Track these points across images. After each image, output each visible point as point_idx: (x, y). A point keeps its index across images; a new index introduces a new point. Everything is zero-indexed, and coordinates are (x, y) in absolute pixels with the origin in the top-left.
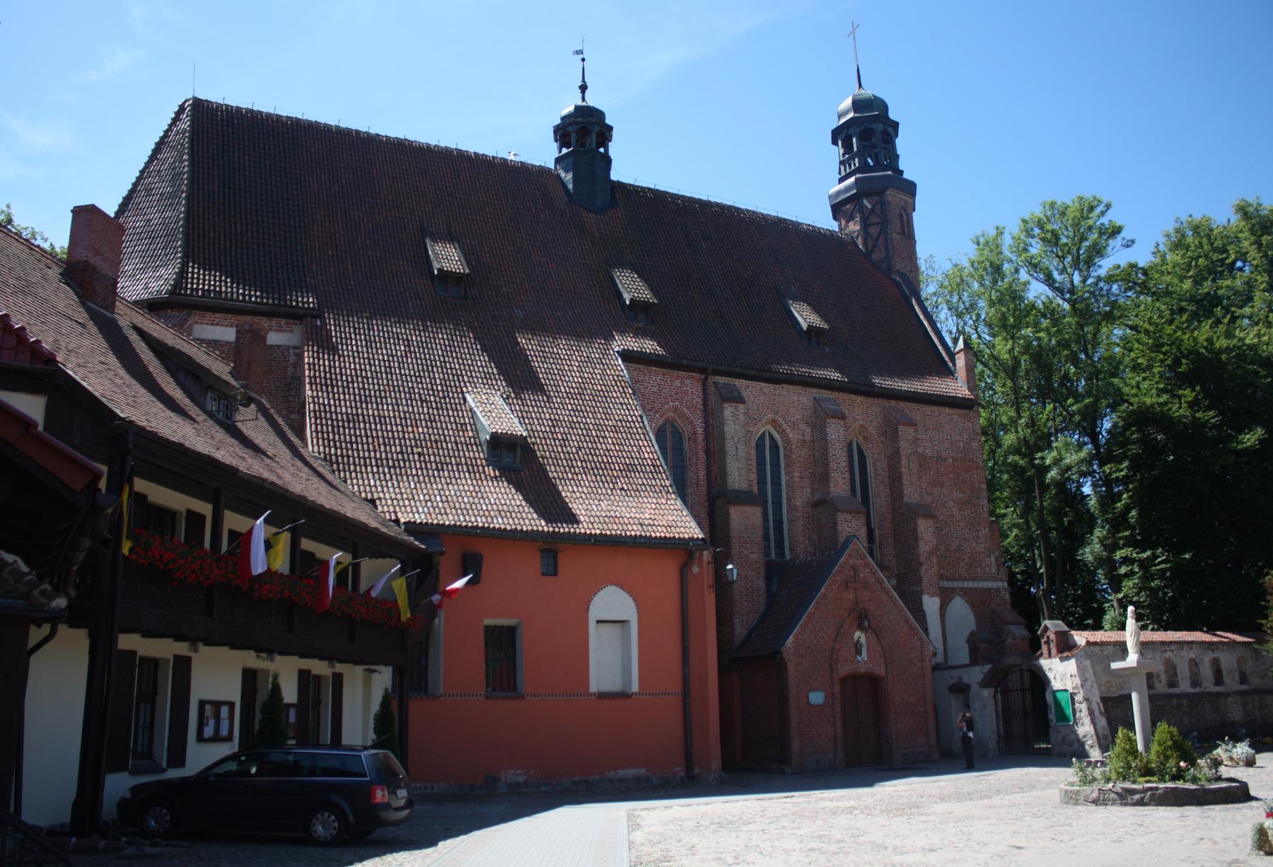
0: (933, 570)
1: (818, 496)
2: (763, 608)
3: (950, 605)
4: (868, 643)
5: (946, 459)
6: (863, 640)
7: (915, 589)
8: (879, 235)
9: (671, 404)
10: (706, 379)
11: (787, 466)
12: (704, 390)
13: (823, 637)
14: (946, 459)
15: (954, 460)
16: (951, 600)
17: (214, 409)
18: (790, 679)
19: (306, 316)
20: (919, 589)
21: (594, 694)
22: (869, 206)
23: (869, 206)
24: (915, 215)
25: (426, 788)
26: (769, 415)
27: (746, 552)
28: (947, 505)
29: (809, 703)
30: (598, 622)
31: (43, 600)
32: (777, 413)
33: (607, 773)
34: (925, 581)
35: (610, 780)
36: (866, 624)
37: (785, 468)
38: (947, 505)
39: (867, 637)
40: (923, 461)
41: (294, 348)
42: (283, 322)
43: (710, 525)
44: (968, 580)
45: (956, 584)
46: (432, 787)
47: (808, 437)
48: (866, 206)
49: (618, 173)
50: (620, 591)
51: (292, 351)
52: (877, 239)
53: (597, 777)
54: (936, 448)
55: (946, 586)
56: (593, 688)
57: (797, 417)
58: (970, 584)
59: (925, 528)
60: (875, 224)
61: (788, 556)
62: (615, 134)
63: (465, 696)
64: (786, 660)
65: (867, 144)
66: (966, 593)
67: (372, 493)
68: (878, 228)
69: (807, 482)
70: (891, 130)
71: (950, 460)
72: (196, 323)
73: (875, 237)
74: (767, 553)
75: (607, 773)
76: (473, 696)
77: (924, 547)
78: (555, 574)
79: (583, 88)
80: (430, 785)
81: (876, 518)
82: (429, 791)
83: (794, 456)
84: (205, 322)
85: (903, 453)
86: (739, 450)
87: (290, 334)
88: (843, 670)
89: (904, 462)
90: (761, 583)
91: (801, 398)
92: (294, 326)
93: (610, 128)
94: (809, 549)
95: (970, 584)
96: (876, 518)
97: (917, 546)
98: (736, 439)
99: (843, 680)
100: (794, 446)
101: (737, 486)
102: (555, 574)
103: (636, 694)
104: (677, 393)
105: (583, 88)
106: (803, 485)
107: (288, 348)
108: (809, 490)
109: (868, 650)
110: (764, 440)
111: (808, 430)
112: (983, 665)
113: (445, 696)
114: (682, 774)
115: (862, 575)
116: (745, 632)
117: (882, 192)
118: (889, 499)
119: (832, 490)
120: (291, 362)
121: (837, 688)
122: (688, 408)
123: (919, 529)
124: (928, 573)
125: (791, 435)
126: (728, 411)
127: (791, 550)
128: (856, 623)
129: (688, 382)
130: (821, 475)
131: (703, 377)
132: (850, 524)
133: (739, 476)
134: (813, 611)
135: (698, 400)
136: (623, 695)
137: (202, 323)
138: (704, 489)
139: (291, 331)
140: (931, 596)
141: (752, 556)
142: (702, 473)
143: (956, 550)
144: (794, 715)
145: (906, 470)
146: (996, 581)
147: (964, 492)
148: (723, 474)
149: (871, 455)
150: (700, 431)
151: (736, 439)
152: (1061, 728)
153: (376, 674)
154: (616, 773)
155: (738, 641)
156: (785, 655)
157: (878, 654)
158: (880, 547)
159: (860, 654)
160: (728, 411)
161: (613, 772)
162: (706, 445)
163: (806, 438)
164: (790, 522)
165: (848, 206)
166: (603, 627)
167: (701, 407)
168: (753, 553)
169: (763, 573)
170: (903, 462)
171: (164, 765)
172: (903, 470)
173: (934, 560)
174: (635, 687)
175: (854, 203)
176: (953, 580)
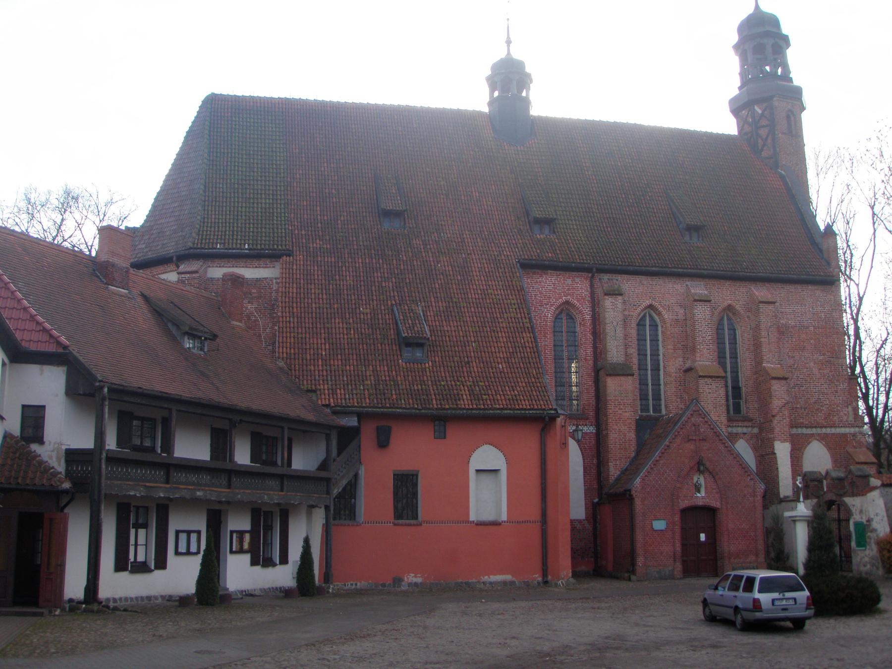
0: (785, 421)
1: (687, 365)
2: (633, 454)
3: (807, 448)
4: (705, 483)
5: (808, 327)
6: (702, 481)
7: (770, 436)
8: (767, 136)
9: (564, 298)
10: (593, 276)
11: (664, 341)
12: (592, 286)
13: (666, 479)
14: (808, 327)
15: (815, 328)
16: (809, 443)
17: (191, 346)
18: (637, 511)
19: (282, 255)
20: (772, 436)
21: (474, 521)
22: (760, 112)
23: (760, 112)
24: (804, 116)
25: (352, 585)
26: (647, 302)
27: (620, 412)
28: (807, 365)
29: (653, 529)
30: (478, 471)
31: (58, 483)
32: (654, 299)
33: (482, 577)
34: (777, 430)
35: (483, 583)
36: (702, 468)
37: (662, 342)
38: (807, 365)
39: (705, 478)
40: (782, 331)
41: (276, 279)
42: (268, 261)
43: (595, 390)
44: (826, 427)
45: (814, 431)
46: (356, 584)
47: (681, 317)
48: (758, 112)
49: (536, 111)
50: (494, 448)
51: (274, 281)
52: (766, 139)
53: (474, 580)
54: (799, 319)
55: (805, 432)
56: (472, 517)
57: (672, 301)
58: (828, 430)
59: (778, 388)
60: (763, 127)
61: (664, 412)
62: (533, 77)
63: (379, 523)
64: (634, 496)
65: (759, 57)
66: (822, 438)
67: (315, 385)
68: (767, 130)
69: (680, 352)
70: (781, 43)
71: (811, 329)
72: (209, 267)
73: (764, 137)
74: (645, 408)
75: (482, 577)
76: (385, 523)
77: (776, 403)
78: (445, 438)
79: (509, 42)
80: (354, 583)
81: (743, 379)
82: (354, 586)
83: (669, 333)
84: (215, 265)
85: (763, 326)
86: (617, 332)
87: (273, 269)
88: (685, 504)
89: (763, 333)
90: (632, 435)
91: (675, 286)
92: (275, 263)
93: (528, 76)
94: (681, 406)
95: (828, 430)
96: (743, 379)
97: (771, 403)
98: (615, 323)
99: (685, 512)
100: (668, 325)
101: (615, 360)
102: (445, 438)
103: (505, 522)
104: (569, 289)
105: (509, 42)
106: (675, 355)
107: (271, 279)
108: (681, 359)
109: (706, 488)
110: (645, 321)
111: (682, 311)
112: (812, 499)
113: (365, 523)
114: (540, 579)
115: (702, 430)
116: (618, 473)
117: (770, 99)
118: (753, 363)
119: (698, 359)
120: (274, 289)
121: (677, 518)
122: (578, 300)
123: (773, 388)
124: (780, 424)
125: (666, 316)
126: (608, 302)
127: (666, 407)
128: (696, 468)
129: (577, 280)
130: (689, 348)
131: (590, 275)
132: (710, 386)
133: (617, 351)
134: (658, 458)
135: (586, 293)
136: (495, 524)
137: (213, 267)
138: (591, 363)
139: (274, 267)
140: (782, 442)
141: (624, 414)
142: (590, 351)
143: (815, 403)
144: (639, 538)
145: (766, 340)
146: (853, 427)
147: (824, 354)
148: (604, 351)
149: (739, 327)
150: (588, 317)
151: (615, 323)
152: (859, 552)
153: (317, 508)
154: (489, 578)
155: (612, 479)
156: (633, 492)
157: (714, 491)
158: (746, 402)
159: (699, 492)
160: (608, 302)
161: (486, 577)
162: (593, 328)
163: (679, 317)
164: (665, 384)
165: (744, 112)
166: (483, 476)
167: (589, 299)
168: (626, 412)
169: (634, 427)
170: (763, 333)
171: (153, 568)
172: (762, 340)
173: (786, 413)
174: (504, 517)
175: (748, 109)
176: (812, 427)
